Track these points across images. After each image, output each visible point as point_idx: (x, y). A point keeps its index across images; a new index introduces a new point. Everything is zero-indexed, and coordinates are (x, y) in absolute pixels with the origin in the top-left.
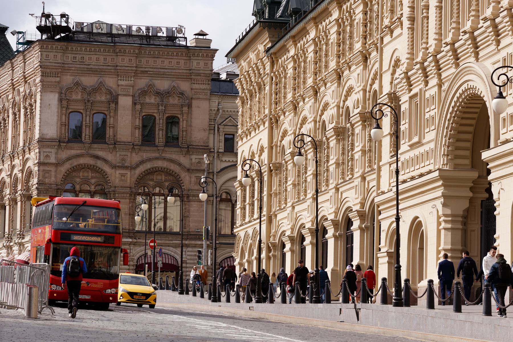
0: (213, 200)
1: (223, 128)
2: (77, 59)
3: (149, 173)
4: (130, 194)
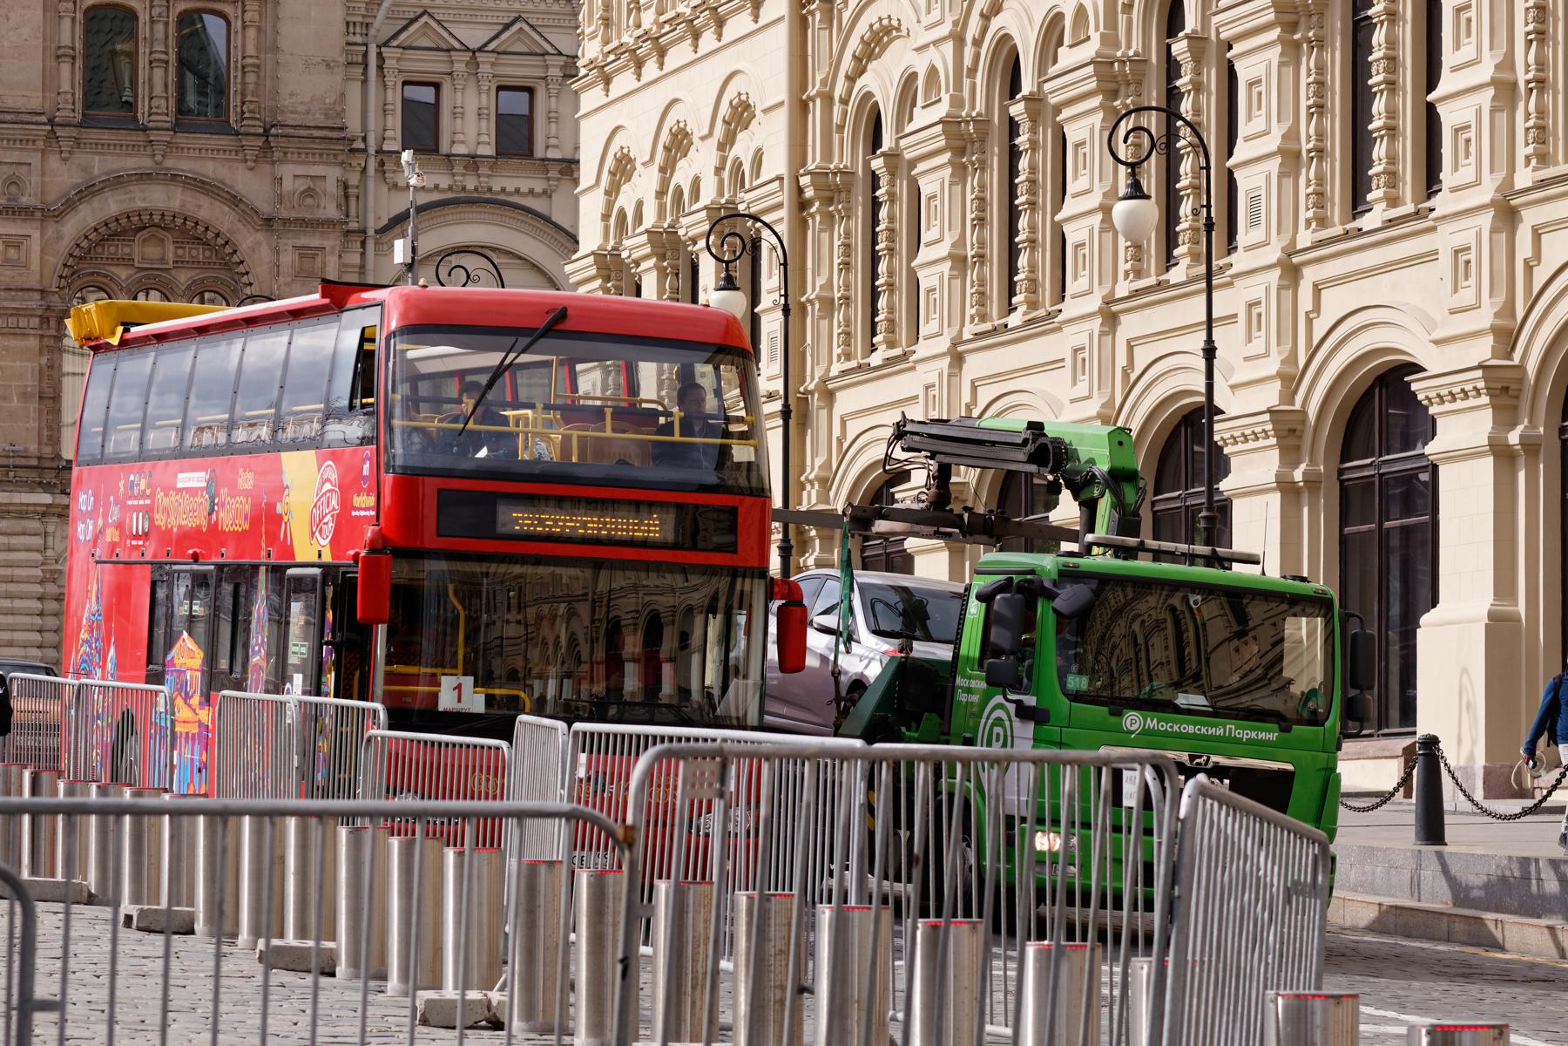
4: (40, 316)
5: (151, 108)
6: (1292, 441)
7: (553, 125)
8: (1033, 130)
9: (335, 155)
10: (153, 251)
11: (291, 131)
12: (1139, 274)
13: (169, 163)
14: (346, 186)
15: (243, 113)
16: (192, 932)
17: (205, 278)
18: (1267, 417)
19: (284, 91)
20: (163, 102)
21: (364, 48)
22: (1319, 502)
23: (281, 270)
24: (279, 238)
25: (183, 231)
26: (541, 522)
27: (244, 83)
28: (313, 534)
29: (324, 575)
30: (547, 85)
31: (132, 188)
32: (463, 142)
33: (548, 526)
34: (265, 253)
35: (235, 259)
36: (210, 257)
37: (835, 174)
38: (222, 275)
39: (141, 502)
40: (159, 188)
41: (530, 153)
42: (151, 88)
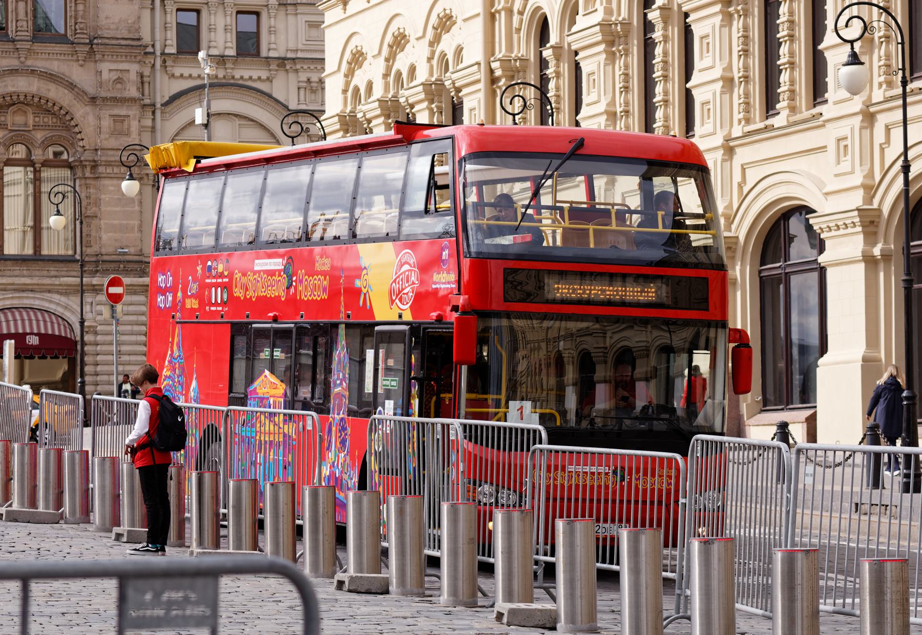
5: (17, 27)
6: (872, 229)
7: (273, 36)
8: (665, 29)
9: (135, 56)
10: (19, 119)
11: (107, 41)
12: (748, 121)
13: (29, 63)
14: (142, 77)
15: (76, 30)
16: (387, 592)
17: (53, 136)
18: (856, 213)
19: (102, 16)
20: (25, 23)
22: (890, 268)
23: (102, 130)
24: (100, 109)
25: (39, 106)
26: (603, 291)
27: (76, 11)
28: (392, 302)
29: (411, 329)
30: (268, 10)
31: (5, 79)
32: (215, 47)
33: (579, 294)
34: (91, 119)
35: (73, 123)
36: (56, 122)
37: (516, 60)
38: (64, 134)
39: (220, 280)
40: (24, 78)
41: (257, 54)
42: (17, 15)
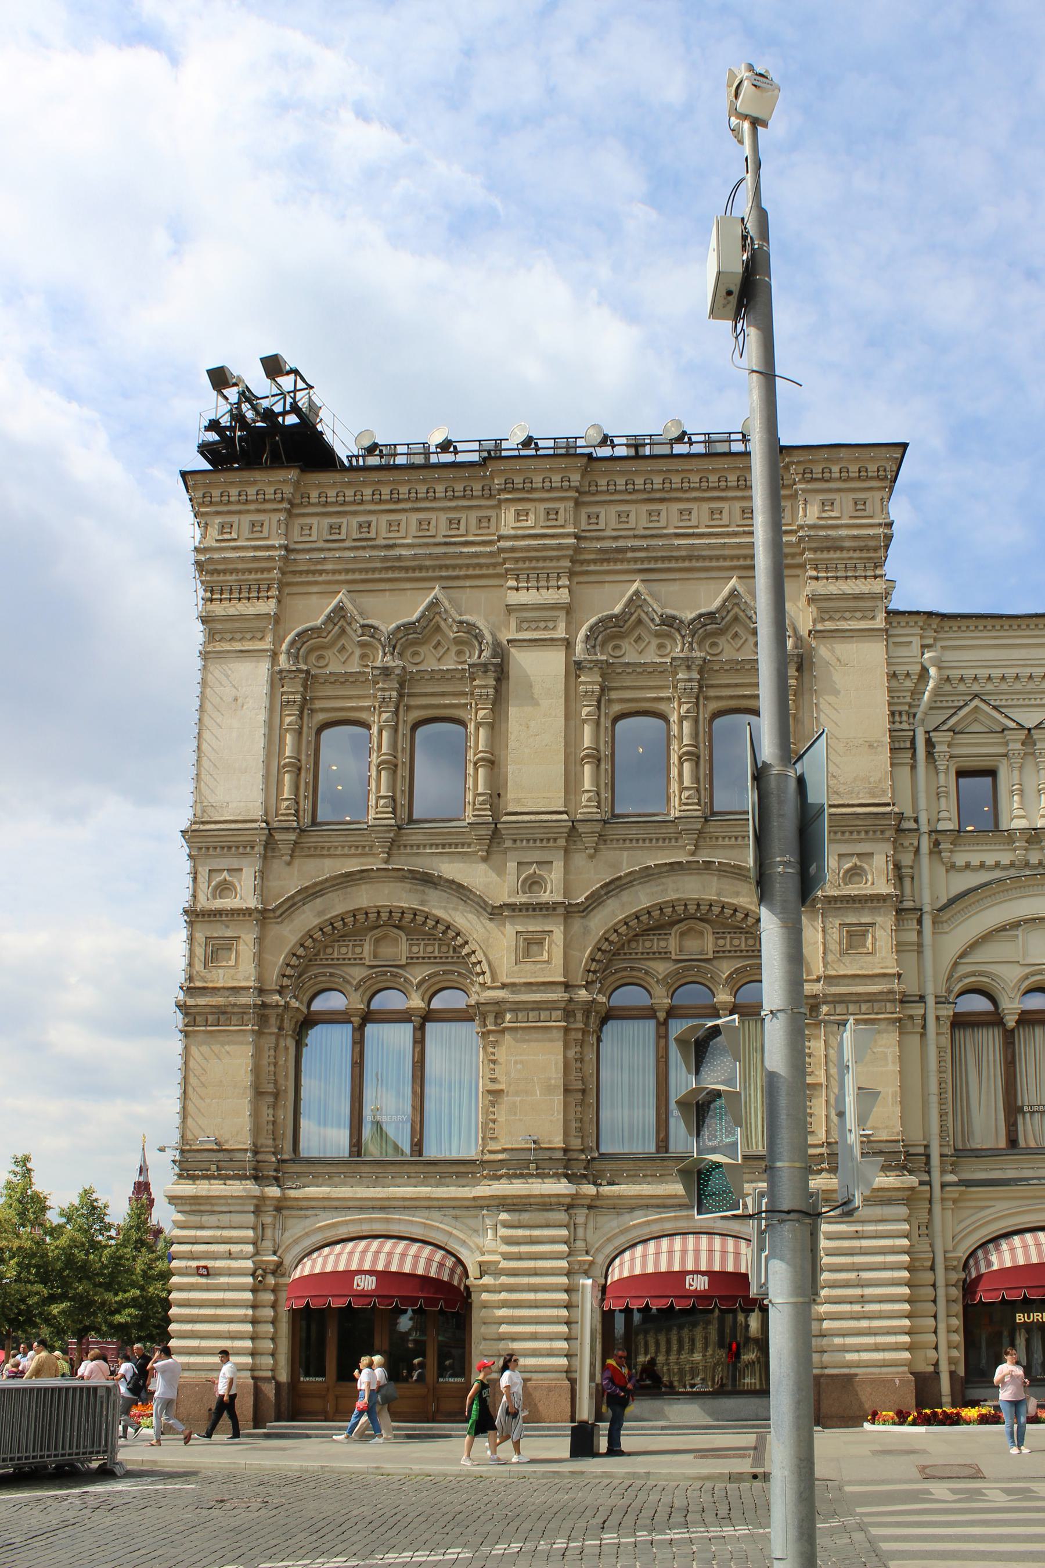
0: (924, 1017)
1: (950, 745)
2: (344, 530)
3: (647, 931)
4: (564, 1009)
21: (912, 733)
31: (664, 880)
